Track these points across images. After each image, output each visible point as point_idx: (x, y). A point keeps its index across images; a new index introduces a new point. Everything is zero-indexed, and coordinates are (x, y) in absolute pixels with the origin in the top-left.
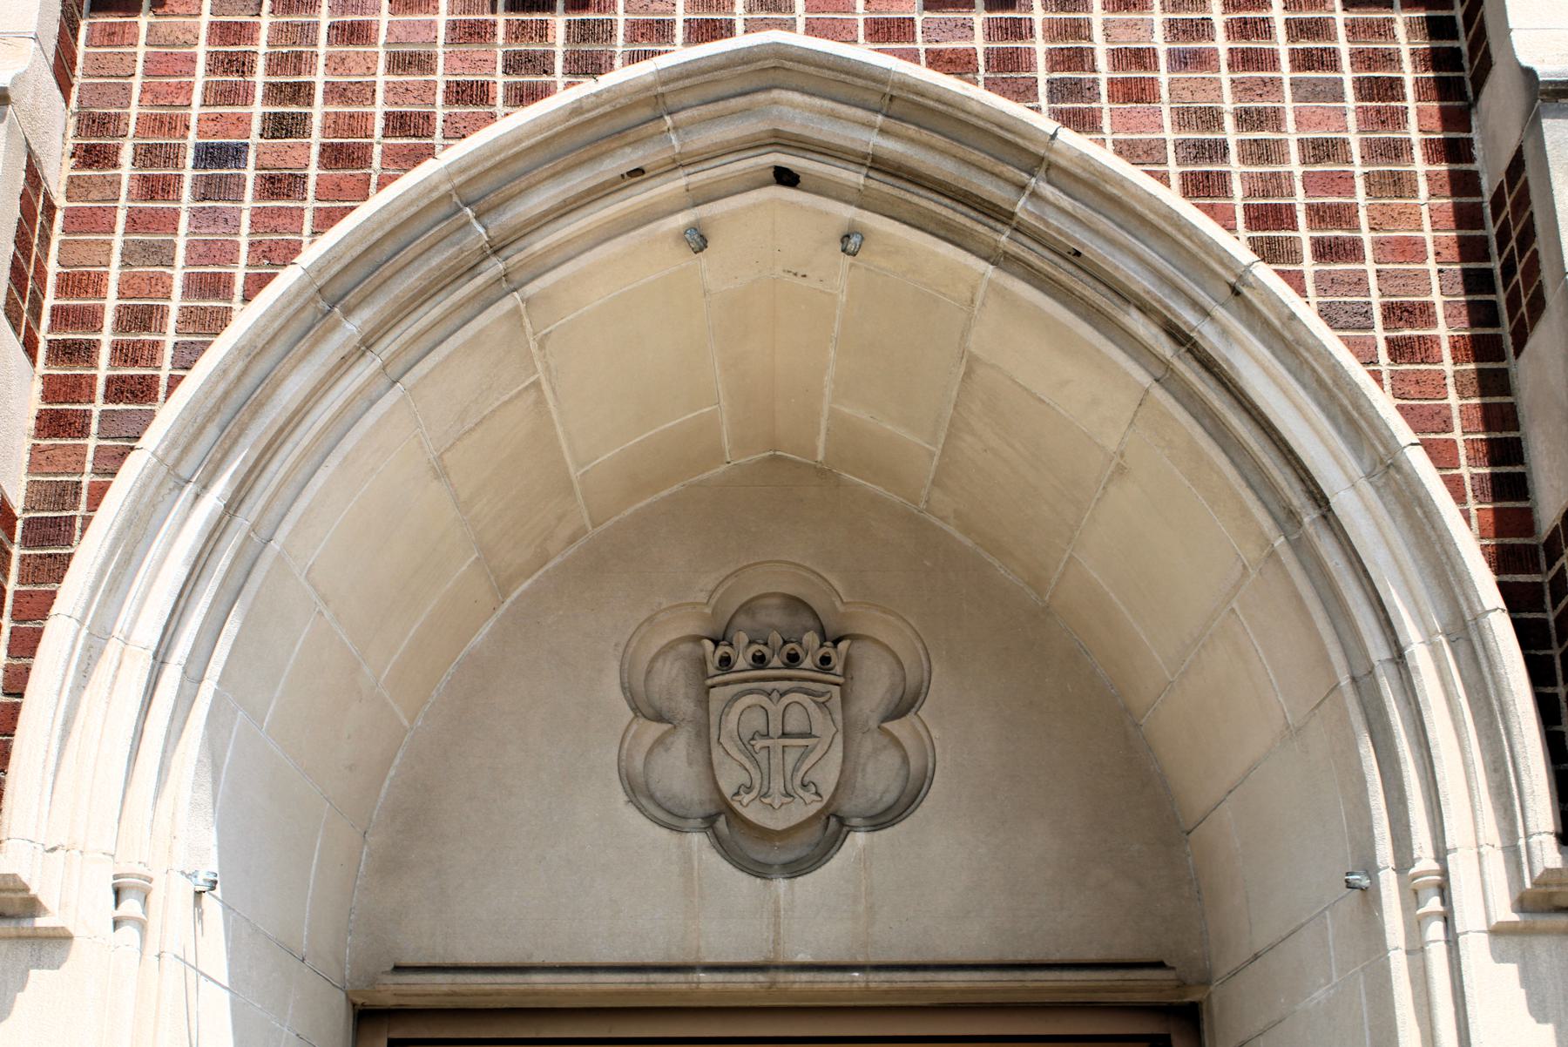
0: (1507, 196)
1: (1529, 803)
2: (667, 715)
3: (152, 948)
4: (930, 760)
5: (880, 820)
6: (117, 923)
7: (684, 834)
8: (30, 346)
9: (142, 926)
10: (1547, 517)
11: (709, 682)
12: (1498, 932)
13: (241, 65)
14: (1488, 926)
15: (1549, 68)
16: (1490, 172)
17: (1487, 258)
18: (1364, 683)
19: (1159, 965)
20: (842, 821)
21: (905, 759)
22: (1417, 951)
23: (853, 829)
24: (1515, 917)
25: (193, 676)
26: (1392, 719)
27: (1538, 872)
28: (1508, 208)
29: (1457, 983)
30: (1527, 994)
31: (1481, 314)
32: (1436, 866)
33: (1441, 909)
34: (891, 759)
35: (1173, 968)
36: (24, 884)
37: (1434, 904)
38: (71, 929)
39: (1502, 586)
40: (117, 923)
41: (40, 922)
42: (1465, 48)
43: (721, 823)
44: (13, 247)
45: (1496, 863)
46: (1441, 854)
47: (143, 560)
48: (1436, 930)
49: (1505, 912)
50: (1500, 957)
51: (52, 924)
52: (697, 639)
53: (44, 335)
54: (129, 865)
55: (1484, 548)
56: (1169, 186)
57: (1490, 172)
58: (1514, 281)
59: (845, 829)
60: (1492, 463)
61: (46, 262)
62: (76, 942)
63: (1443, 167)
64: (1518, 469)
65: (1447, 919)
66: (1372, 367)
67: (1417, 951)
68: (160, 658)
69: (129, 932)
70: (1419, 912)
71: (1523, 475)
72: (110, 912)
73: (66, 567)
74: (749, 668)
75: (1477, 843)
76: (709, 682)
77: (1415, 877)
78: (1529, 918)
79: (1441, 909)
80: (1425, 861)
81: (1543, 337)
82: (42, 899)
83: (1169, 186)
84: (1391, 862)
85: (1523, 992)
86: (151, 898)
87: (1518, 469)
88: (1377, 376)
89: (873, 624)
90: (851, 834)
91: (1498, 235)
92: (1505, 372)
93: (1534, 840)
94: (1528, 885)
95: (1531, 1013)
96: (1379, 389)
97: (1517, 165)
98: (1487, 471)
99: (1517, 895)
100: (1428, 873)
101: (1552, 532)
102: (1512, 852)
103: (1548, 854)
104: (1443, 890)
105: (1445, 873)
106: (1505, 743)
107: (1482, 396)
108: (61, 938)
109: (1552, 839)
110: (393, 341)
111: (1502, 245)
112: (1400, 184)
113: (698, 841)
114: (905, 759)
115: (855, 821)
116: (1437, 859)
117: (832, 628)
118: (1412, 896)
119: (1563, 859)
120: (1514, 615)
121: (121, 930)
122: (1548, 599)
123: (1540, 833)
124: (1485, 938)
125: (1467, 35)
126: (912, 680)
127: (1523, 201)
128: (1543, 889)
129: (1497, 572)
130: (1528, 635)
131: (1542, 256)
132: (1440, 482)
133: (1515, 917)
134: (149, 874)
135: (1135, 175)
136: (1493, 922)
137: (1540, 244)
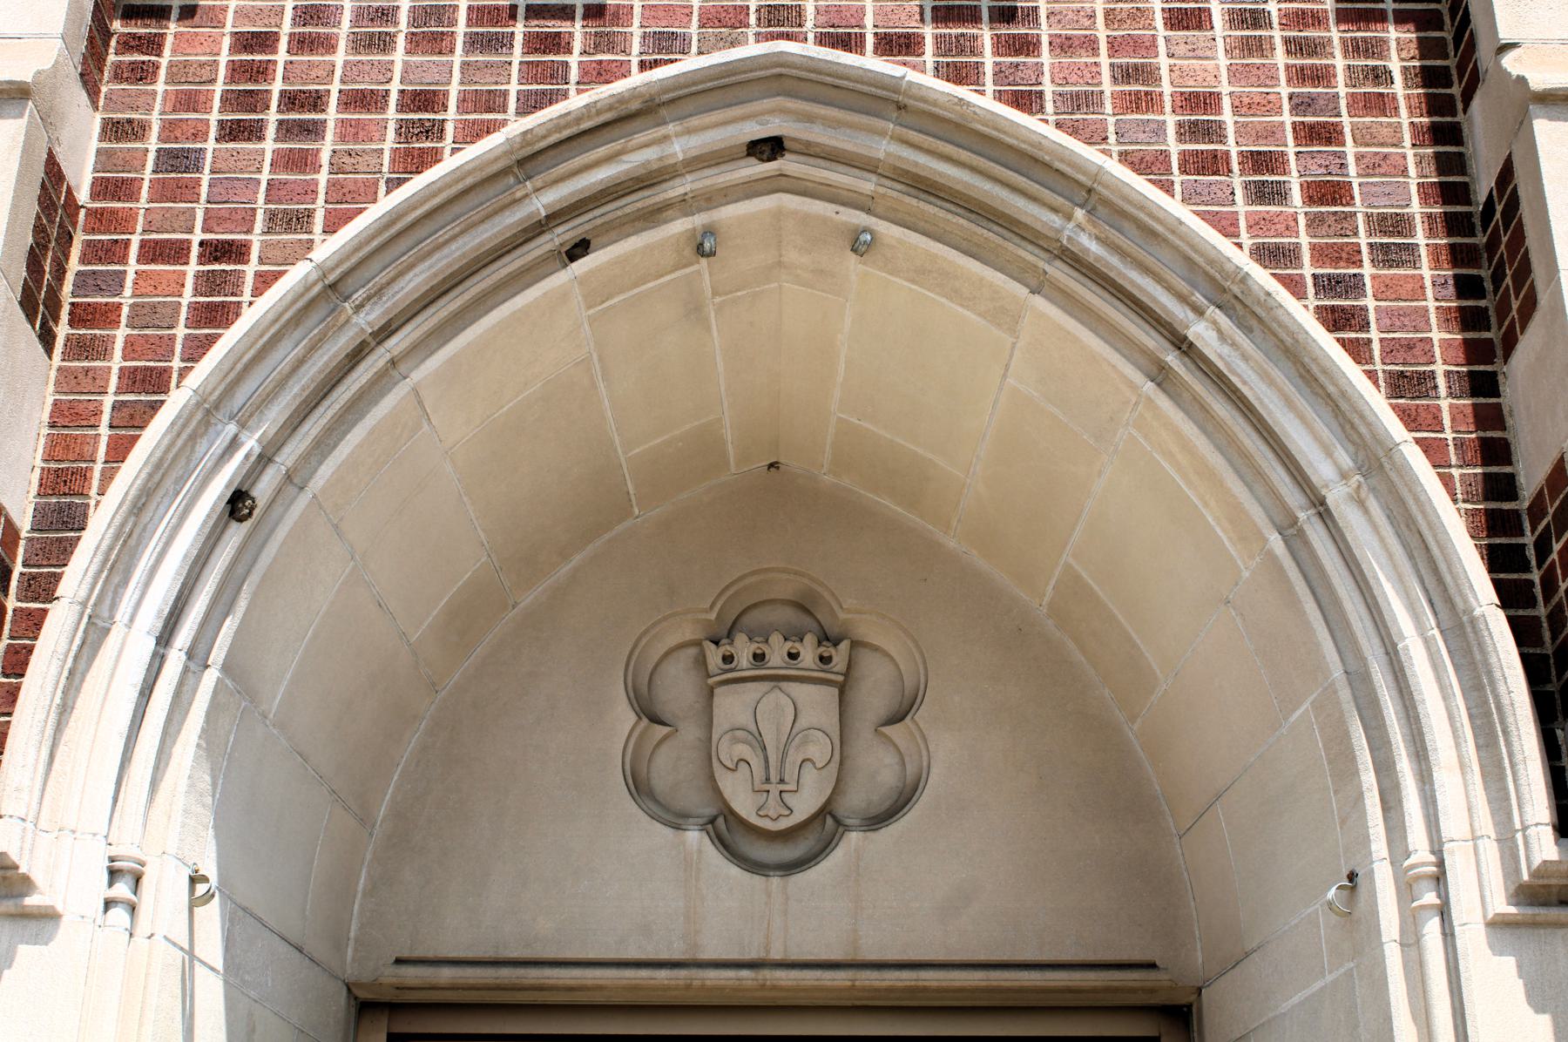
0: (1497, 203)
1: (1524, 789)
2: (666, 717)
3: (144, 926)
4: (925, 758)
5: (878, 820)
6: (109, 904)
7: (681, 831)
8: (47, 339)
9: (133, 909)
10: (1531, 474)
11: (711, 681)
12: (1498, 925)
13: (255, 101)
14: (1485, 917)
15: (1539, 80)
16: (1484, 184)
17: (1527, 569)
18: (1359, 679)
19: (1152, 966)
20: (838, 822)
21: (903, 763)
22: (1411, 942)
23: (848, 828)
24: (1513, 910)
25: (197, 657)
26: (1385, 712)
27: (1536, 862)
28: (1498, 215)
29: (1457, 1005)
30: (1525, 985)
31: (1466, 287)
32: (1433, 859)
33: (1438, 901)
34: (889, 759)
35: (1166, 969)
36: (14, 863)
37: (1430, 898)
38: (60, 908)
39: (1498, 585)
40: (109, 904)
41: (31, 901)
42: (1537, 581)
43: (720, 821)
44: (25, 274)
45: (1491, 852)
46: (1438, 851)
47: (190, 476)
48: (1432, 927)
49: (1501, 905)
50: (1497, 950)
51: (41, 903)
52: (697, 643)
53: (62, 330)
54: (127, 847)
55: (1470, 514)
56: (1173, 196)
57: (1484, 184)
58: (1504, 286)
59: (841, 829)
60: (1450, 234)
61: (67, 263)
62: (64, 919)
63: (1437, 210)
64: (1507, 469)
65: (1444, 912)
66: (1367, 367)
67: (1411, 942)
68: (147, 691)
69: (119, 915)
70: (1415, 904)
71: (1466, 185)
72: (102, 890)
73: (38, 626)
74: (750, 666)
75: (1473, 831)
76: (711, 681)
77: (1413, 867)
78: (1530, 911)
79: (1438, 901)
80: (1421, 853)
81: (1530, 343)
82: (33, 876)
83: (1173, 196)
84: (1385, 853)
85: (1521, 982)
86: (145, 881)
87: (1507, 469)
88: (1371, 375)
89: (869, 630)
90: (847, 833)
91: (1536, 544)
92: (1494, 374)
93: (1531, 831)
94: (1526, 877)
95: (1529, 1004)
96: (1377, 391)
97: (1506, 174)
98: (1479, 470)
99: (1512, 888)
100: (1423, 864)
101: (1537, 495)
102: (1507, 841)
103: (1544, 847)
104: (1439, 879)
105: (1441, 864)
106: (1504, 750)
107: (1484, 464)
108: (48, 917)
109: (1549, 829)
110: (141, 1025)
111: (1541, 558)
112: (1381, 104)
113: (694, 837)
114: (903, 763)
115: (849, 822)
116: (1433, 852)
117: (833, 631)
118: (1406, 888)
119: (1559, 853)
120: (1512, 612)
121: (113, 912)
122: (1554, 672)
123: (1537, 825)
124: (1482, 927)
125: (1460, 83)
126: (909, 683)
127: (1513, 204)
128: (1541, 882)
129: (1490, 571)
130: (1523, 632)
131: (1521, 192)
132: (1436, 475)
133: (1513, 910)
134: (143, 858)
135: (1140, 185)
136: (1490, 916)
137: (1525, 210)
